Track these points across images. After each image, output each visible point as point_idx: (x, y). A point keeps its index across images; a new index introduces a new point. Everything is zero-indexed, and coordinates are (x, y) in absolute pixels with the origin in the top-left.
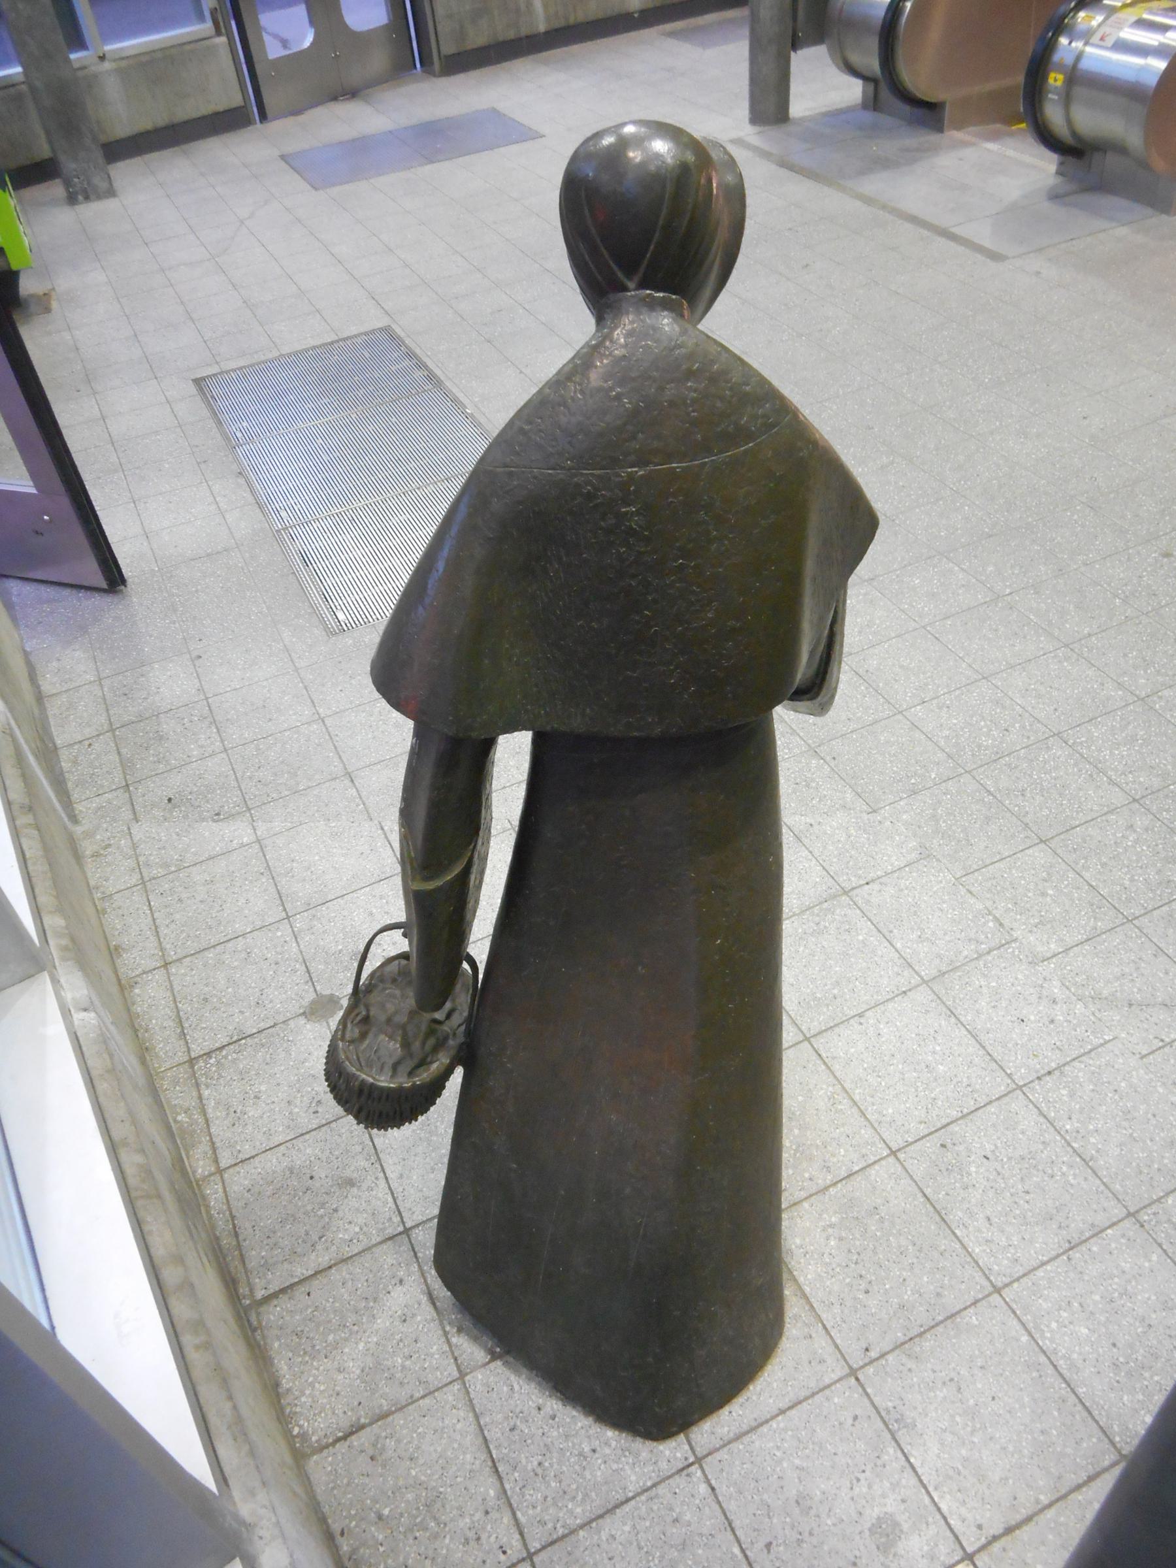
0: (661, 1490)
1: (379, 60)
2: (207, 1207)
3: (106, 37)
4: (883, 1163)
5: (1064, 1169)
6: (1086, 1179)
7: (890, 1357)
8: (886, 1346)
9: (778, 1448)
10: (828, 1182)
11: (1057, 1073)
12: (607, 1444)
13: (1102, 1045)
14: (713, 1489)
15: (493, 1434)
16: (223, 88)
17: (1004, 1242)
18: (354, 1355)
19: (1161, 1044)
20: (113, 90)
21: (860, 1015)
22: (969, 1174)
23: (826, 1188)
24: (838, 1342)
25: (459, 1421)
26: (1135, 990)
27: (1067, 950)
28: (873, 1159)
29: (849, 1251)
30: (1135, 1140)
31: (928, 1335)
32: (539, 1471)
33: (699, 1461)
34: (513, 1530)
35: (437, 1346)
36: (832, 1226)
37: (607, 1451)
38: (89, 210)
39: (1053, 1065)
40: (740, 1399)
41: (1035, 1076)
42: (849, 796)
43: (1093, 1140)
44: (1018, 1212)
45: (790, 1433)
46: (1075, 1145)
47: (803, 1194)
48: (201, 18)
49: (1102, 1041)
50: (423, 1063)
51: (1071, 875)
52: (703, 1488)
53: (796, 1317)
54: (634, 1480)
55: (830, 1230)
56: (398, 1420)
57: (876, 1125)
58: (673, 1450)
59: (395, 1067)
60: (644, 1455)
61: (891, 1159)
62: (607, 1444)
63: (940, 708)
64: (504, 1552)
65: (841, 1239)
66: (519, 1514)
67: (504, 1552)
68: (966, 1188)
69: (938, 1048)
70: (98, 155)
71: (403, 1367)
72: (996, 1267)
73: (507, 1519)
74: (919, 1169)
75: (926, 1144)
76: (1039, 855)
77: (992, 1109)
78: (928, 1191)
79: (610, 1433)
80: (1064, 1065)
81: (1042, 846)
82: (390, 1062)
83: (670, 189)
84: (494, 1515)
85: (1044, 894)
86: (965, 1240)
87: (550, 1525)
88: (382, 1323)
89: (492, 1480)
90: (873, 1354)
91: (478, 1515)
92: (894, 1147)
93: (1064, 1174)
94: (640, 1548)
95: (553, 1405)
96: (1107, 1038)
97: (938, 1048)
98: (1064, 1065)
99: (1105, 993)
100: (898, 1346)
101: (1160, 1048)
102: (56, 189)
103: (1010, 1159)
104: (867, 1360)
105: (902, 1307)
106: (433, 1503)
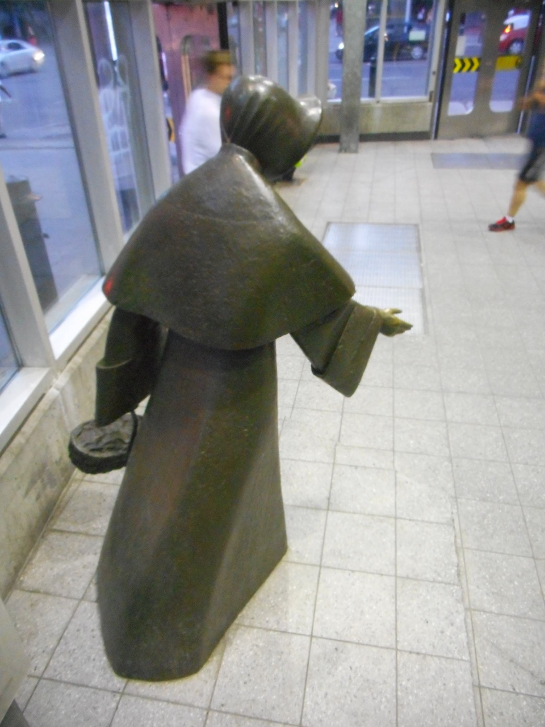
0: (101, 693)
1: (501, 126)
2: (68, 489)
3: (384, 95)
4: (304, 637)
5: (384, 700)
6: (390, 712)
7: (228, 717)
8: (232, 710)
9: (153, 714)
10: (273, 628)
11: (422, 656)
12: (100, 661)
13: (458, 660)
14: (117, 708)
15: (72, 627)
16: (423, 123)
17: (324, 709)
18: (59, 568)
19: (512, 690)
20: (377, 114)
21: (353, 571)
22: (336, 669)
23: (270, 630)
24: (215, 693)
25: (66, 614)
26: (521, 656)
27: (499, 614)
28: (300, 632)
29: (254, 662)
30: (433, 713)
31: (252, 721)
32: (71, 652)
33: (122, 694)
34: (45, 665)
35: (84, 583)
36: (257, 646)
37: (98, 664)
38: (344, 156)
39: (424, 651)
40: (158, 684)
41: (409, 649)
42: (450, 485)
43: (410, 698)
44: (343, 701)
45: (163, 712)
46: (399, 693)
47: (258, 625)
48: (426, 93)
49: (460, 658)
50: (100, 450)
51: (535, 582)
52: (114, 705)
53: (209, 671)
54: (96, 681)
55: (255, 648)
56: (50, 599)
57: (316, 619)
58: (118, 682)
59: (87, 445)
60: (108, 676)
61: (308, 639)
62: (100, 661)
63: (533, 470)
64: (35, 670)
65: (256, 654)
66: (52, 661)
67: (35, 670)
68: (329, 673)
69: (374, 607)
70: (357, 138)
71: (69, 583)
72: (309, 717)
73: (46, 659)
74: (316, 650)
75: (330, 643)
76: (526, 563)
77: (375, 650)
78: (311, 663)
79: (105, 658)
80: (429, 655)
81: (532, 560)
82: (88, 441)
83: (255, 110)
84: (45, 654)
85: (511, 582)
86: (307, 695)
87: (56, 673)
88: (77, 563)
89: (55, 642)
90: (223, 709)
91: (40, 651)
92: (315, 634)
93: (381, 702)
94: (74, 707)
95: (98, 633)
96: (464, 658)
97: (374, 607)
98: (429, 655)
99: (503, 646)
100: (236, 714)
101: (509, 692)
102: (336, 146)
103: (361, 676)
104: (218, 709)
105: (254, 700)
106: (32, 634)
